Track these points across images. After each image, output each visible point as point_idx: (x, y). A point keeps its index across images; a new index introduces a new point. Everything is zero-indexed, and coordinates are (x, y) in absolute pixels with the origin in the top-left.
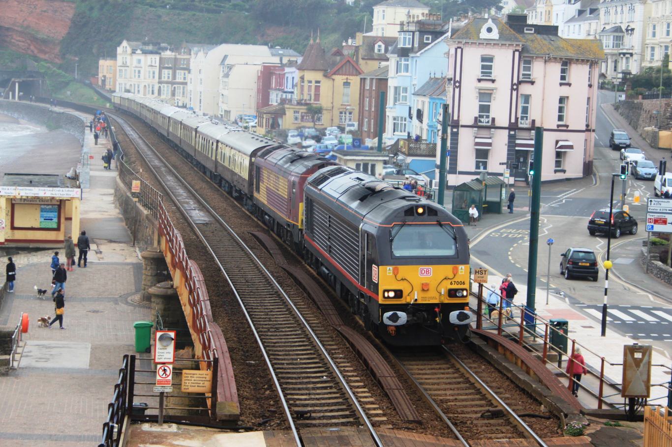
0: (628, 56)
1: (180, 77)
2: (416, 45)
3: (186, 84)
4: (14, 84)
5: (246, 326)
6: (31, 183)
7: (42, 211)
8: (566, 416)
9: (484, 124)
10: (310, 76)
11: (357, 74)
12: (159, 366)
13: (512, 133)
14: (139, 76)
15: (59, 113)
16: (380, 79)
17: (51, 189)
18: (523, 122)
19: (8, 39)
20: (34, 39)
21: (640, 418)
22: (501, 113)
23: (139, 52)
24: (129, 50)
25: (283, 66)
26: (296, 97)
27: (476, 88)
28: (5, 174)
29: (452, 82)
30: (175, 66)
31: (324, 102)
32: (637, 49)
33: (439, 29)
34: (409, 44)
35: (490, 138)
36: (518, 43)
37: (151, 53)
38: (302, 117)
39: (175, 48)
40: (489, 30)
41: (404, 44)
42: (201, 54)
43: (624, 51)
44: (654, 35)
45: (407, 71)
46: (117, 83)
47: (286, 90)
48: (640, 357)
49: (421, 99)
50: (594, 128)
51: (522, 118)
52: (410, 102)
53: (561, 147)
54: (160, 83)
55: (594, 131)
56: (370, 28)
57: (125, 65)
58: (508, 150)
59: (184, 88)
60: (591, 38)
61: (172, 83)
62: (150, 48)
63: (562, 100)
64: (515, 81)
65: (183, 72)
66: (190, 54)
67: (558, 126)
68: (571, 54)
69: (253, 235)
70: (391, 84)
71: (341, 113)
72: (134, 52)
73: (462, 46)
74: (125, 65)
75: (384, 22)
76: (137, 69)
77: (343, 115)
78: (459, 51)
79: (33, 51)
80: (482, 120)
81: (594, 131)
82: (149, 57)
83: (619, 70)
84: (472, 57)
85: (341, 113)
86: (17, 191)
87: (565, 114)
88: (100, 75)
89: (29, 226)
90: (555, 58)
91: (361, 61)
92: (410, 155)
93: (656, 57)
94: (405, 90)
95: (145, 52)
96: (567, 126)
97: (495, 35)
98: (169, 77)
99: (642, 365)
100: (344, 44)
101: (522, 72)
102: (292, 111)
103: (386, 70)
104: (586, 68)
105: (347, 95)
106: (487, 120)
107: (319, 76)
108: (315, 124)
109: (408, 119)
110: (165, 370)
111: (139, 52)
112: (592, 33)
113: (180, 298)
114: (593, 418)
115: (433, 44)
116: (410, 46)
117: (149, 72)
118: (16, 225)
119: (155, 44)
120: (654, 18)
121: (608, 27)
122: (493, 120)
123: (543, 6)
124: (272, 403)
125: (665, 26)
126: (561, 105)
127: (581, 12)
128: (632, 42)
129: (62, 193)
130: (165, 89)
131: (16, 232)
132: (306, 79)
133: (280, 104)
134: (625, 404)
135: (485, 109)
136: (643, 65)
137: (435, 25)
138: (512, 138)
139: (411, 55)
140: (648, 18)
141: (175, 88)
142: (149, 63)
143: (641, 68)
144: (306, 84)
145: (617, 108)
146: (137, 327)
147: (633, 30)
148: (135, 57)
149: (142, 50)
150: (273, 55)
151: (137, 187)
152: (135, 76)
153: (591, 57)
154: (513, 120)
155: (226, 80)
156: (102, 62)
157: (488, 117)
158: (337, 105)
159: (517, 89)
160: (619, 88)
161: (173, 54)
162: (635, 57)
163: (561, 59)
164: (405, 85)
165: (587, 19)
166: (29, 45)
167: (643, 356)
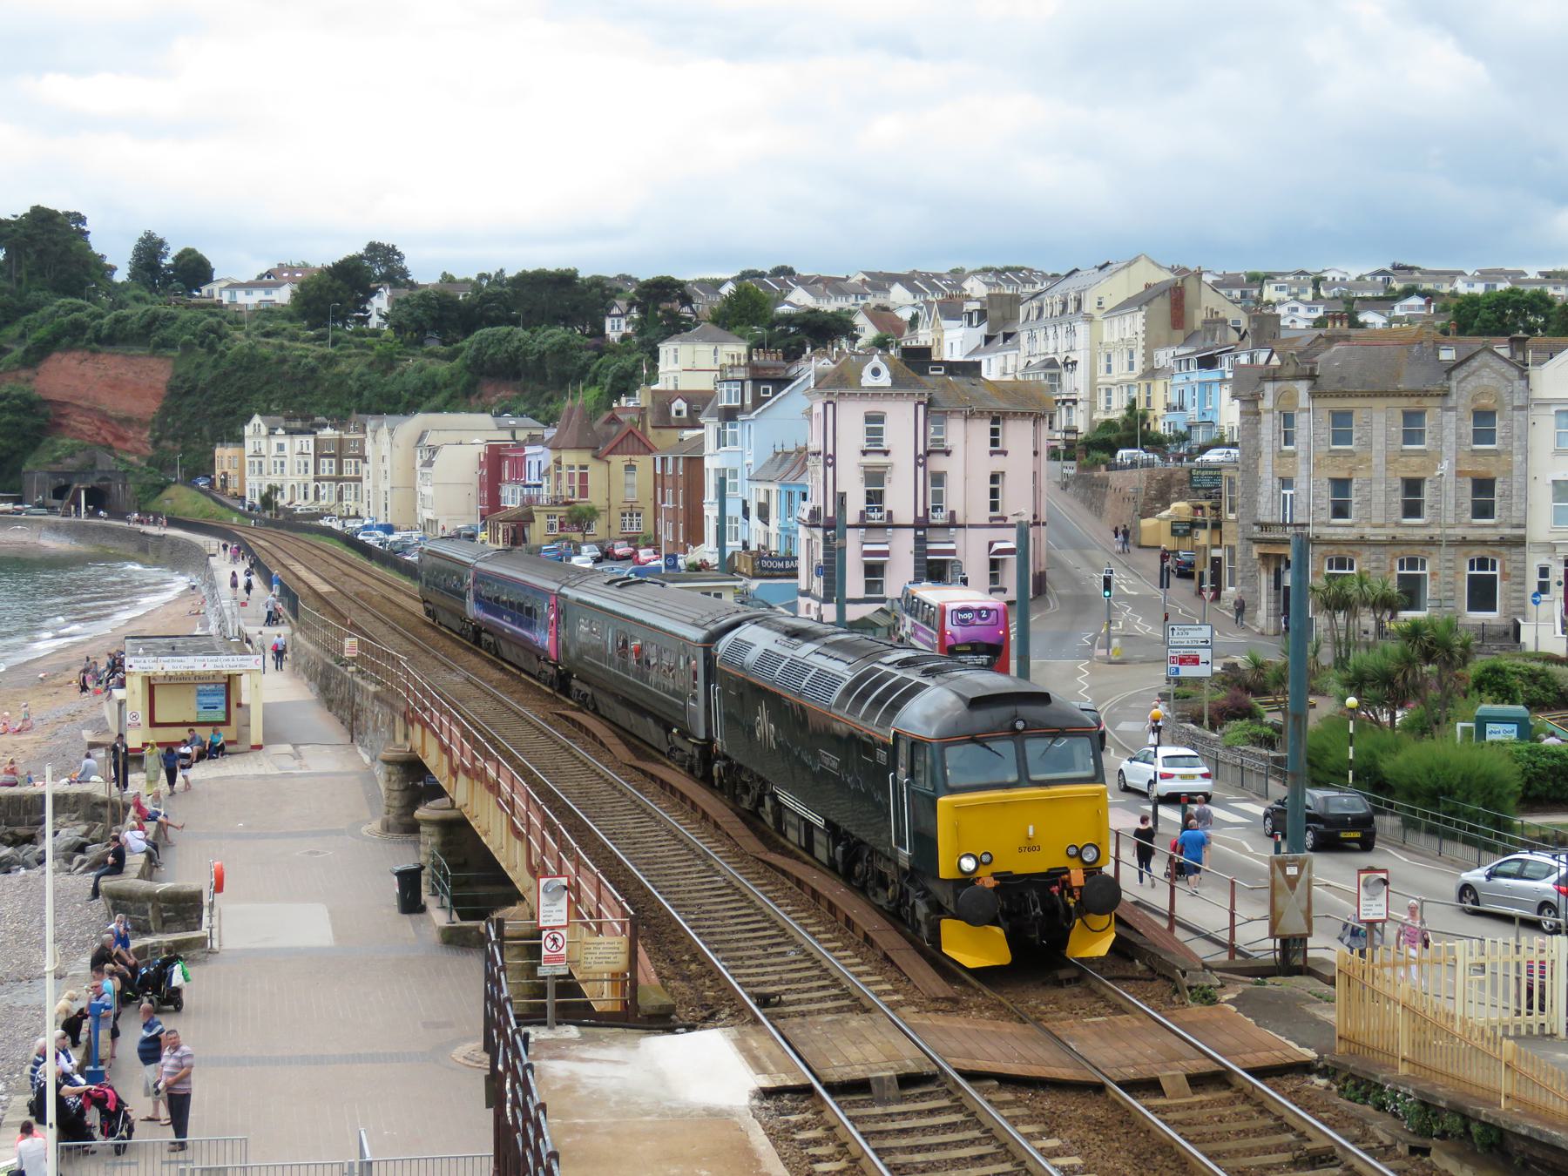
0: (1070, 404)
1: (349, 471)
2: (748, 402)
3: (360, 480)
4: (78, 492)
5: (615, 863)
6: (174, 651)
7: (199, 695)
8: (1184, 974)
9: (876, 522)
10: (569, 458)
11: (642, 449)
12: (544, 934)
13: (920, 533)
14: (282, 471)
15: (159, 536)
16: (690, 458)
17: (214, 658)
18: (936, 515)
19: (64, 422)
20: (105, 418)
21: (1305, 970)
22: (901, 500)
23: (280, 431)
24: (264, 430)
25: (520, 446)
26: (546, 493)
27: (860, 465)
28: (127, 638)
29: (821, 457)
30: (339, 452)
31: (596, 498)
32: (1083, 393)
33: (781, 374)
34: (736, 401)
35: (952, 542)
36: (921, 391)
37: (301, 432)
38: (562, 524)
39: (340, 422)
40: (876, 372)
41: (729, 400)
42: (384, 433)
43: (1064, 397)
44: (1109, 369)
45: (735, 444)
46: (247, 483)
47: (528, 482)
48: (1296, 873)
49: (763, 487)
50: (1044, 519)
51: (935, 509)
52: (743, 491)
53: (997, 552)
54: (316, 480)
55: (1044, 524)
56: (653, 377)
57: (257, 454)
58: (916, 561)
59: (356, 487)
60: (1009, 378)
61: (338, 480)
62: (298, 424)
63: (994, 478)
64: (921, 451)
65: (353, 461)
66: (365, 432)
67: (991, 519)
68: (1003, 405)
69: (560, 715)
70: (710, 464)
71: (624, 515)
72: (272, 432)
73: (834, 400)
74: (257, 454)
75: (677, 367)
76: (278, 460)
77: (628, 517)
78: (830, 407)
79: (105, 439)
80: (872, 515)
81: (1044, 524)
82: (298, 439)
83: (1057, 426)
84: (851, 417)
85: (624, 515)
86: (160, 665)
87: (1000, 500)
88: (218, 472)
89: (180, 720)
90: (981, 413)
91: (650, 431)
92: (755, 577)
93: (1114, 405)
94: (734, 473)
95: (290, 432)
96: (1005, 519)
97: (885, 380)
98: (331, 471)
99: (1298, 885)
100: (615, 405)
101: (930, 437)
102: (544, 516)
103: (699, 443)
104: (1028, 425)
105: (632, 485)
106: (879, 515)
107: (585, 457)
108: (584, 535)
109: (741, 519)
110: (554, 940)
111: (280, 431)
112: (1009, 370)
113: (473, 824)
114: (1227, 975)
115: (775, 399)
116: (739, 404)
117: (299, 463)
118: (158, 719)
119: (305, 419)
120: (1107, 344)
121: (1034, 361)
122: (890, 513)
123: (929, 331)
124: (708, 983)
125: (1126, 356)
126: (994, 486)
127: (988, 339)
128: (1074, 383)
129: (232, 663)
130: (326, 490)
131: (158, 730)
132: (564, 462)
133: (523, 505)
134: (1275, 950)
135: (874, 498)
136: (1095, 417)
137: (775, 368)
138: (920, 541)
139: (740, 417)
140: (1096, 344)
141: (342, 487)
142: (298, 449)
143: (1092, 422)
144: (564, 472)
145: (1065, 486)
146: (400, 874)
147: (1074, 363)
148: (275, 441)
149: (284, 428)
150: (500, 428)
151: (352, 648)
152: (299, 471)
153: (1035, 409)
154: (921, 514)
155: (426, 470)
156: (219, 451)
157: (880, 510)
158: (617, 500)
159: (924, 465)
160: (1069, 456)
161: (337, 432)
162: (1081, 405)
163: (990, 413)
164: (733, 466)
165: (1000, 350)
166: (100, 429)
167: (1300, 870)
